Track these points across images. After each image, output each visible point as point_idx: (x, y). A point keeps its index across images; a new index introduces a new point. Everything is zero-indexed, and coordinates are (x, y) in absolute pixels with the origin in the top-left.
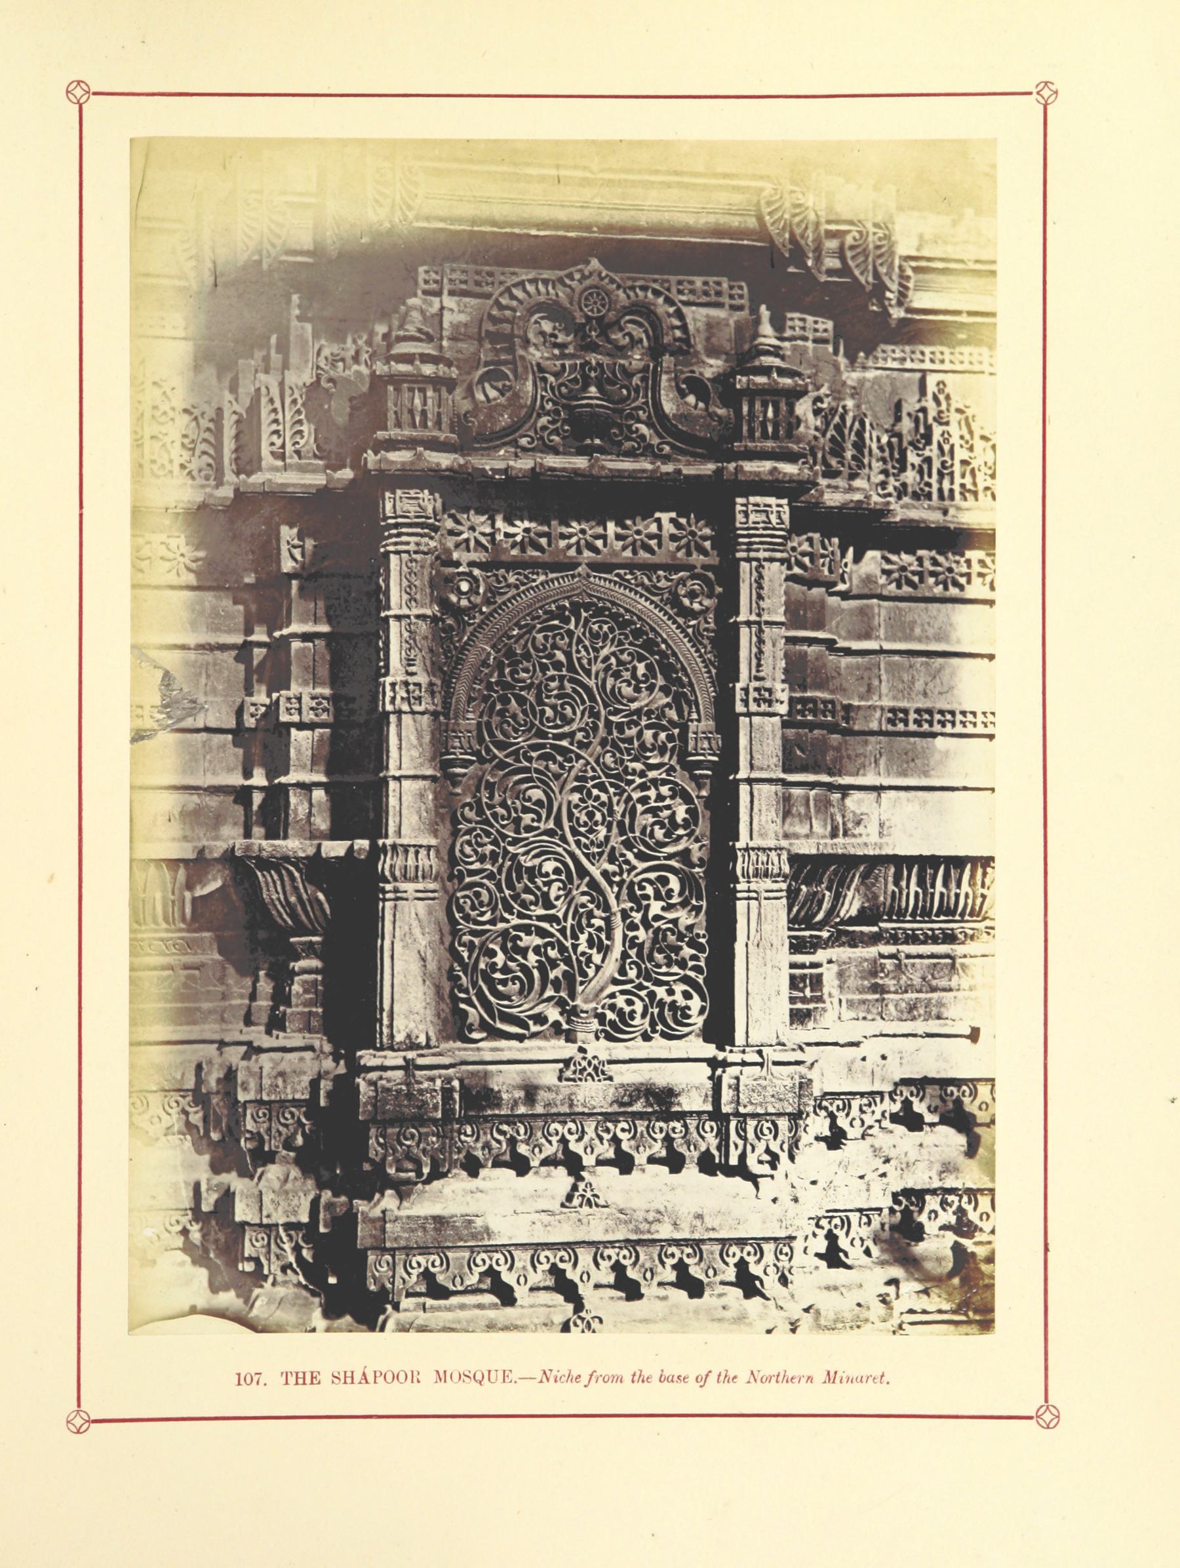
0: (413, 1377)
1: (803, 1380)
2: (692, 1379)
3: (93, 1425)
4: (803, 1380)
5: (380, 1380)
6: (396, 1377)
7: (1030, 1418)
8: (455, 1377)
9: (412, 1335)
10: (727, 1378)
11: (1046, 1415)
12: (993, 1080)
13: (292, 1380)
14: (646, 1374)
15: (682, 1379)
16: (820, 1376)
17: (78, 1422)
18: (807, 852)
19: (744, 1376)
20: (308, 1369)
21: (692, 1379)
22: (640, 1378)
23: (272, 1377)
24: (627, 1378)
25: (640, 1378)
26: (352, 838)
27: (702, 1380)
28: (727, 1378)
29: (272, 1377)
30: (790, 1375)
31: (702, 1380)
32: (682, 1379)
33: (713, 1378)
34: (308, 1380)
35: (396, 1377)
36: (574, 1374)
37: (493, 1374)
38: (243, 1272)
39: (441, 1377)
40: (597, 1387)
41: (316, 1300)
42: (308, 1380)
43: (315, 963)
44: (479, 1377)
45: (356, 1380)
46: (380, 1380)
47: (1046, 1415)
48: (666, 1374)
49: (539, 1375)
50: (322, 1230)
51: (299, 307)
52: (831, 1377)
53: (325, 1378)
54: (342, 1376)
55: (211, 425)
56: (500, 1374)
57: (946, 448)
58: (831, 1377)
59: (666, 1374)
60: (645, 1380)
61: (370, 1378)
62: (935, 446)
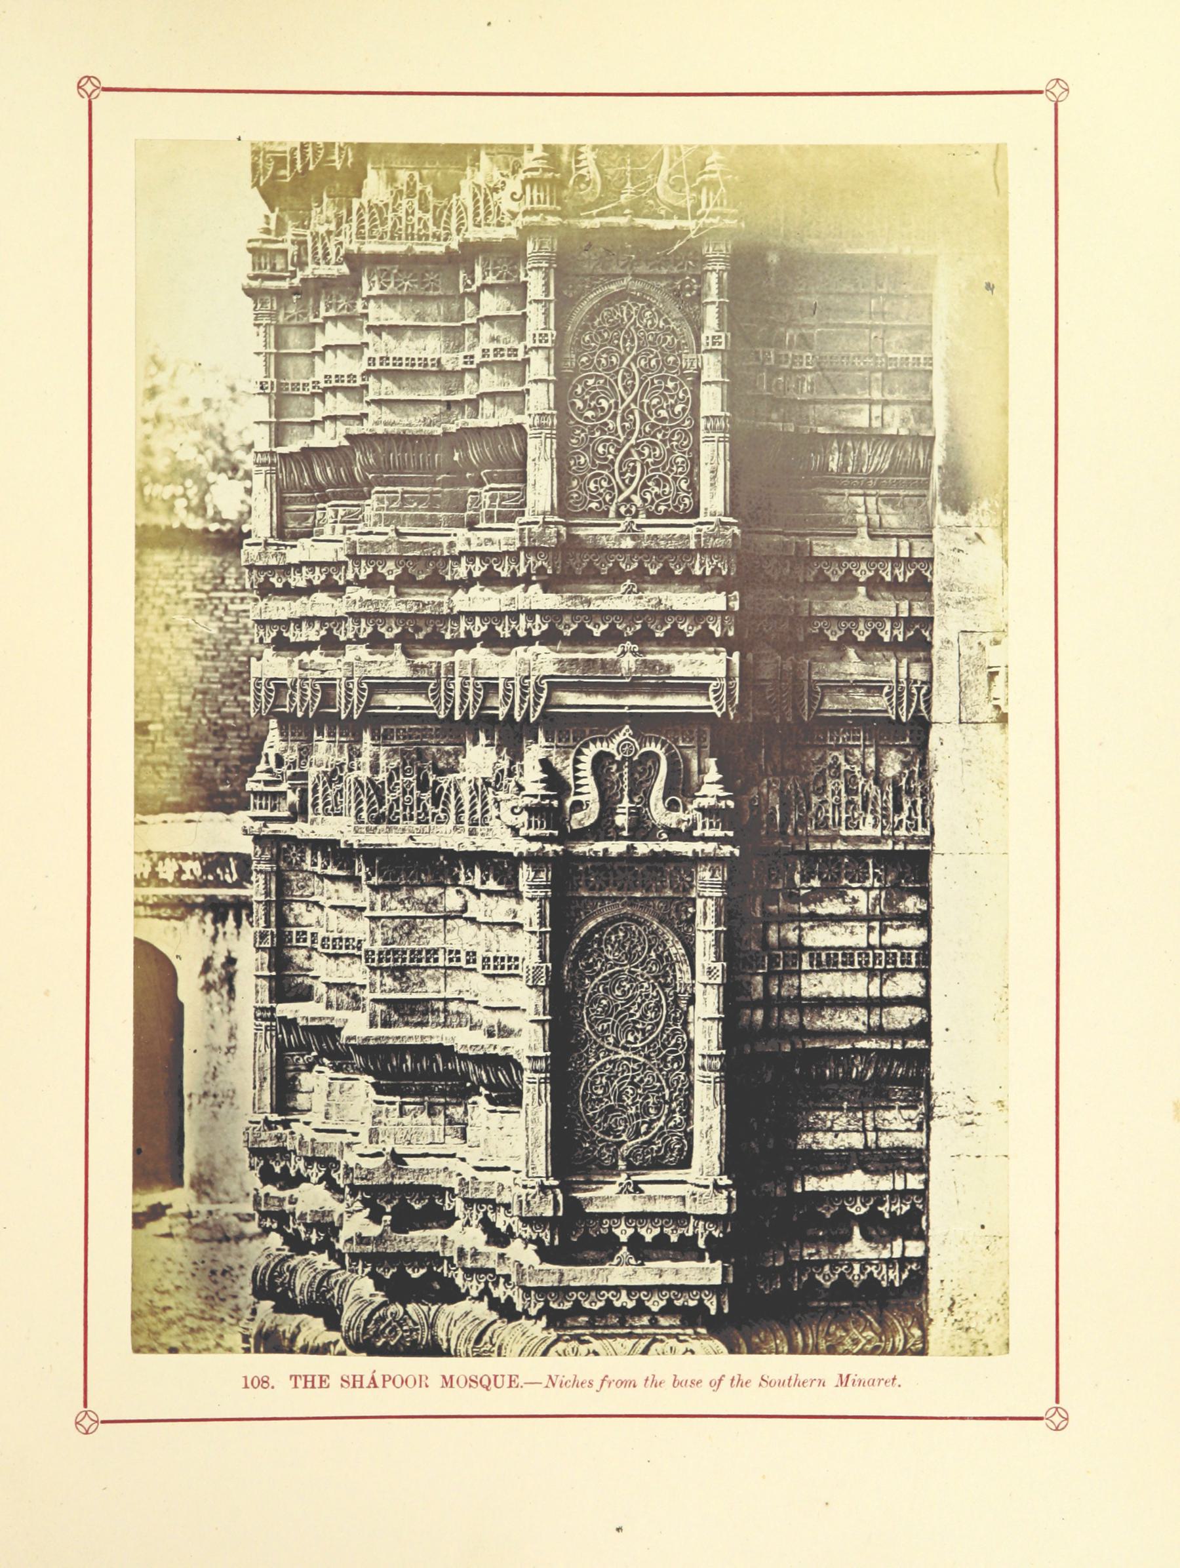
1: (815, 1383)
2: (706, 1383)
3: (86, 99)
4: (815, 1383)
5: (389, 1384)
6: (405, 1382)
7: (85, 1405)
8: (398, 1382)
11: (1056, 1417)
13: (301, 1383)
14: (744, 1379)
15: (696, 1383)
17: (1057, 1419)
20: (317, 1373)
21: (706, 1383)
24: (640, 1382)
26: (893, 850)
30: (801, 1378)
32: (696, 1383)
33: (726, 1383)
34: (317, 1383)
35: (405, 1382)
37: (499, 1379)
42: (317, 1383)
44: (485, 1382)
45: (366, 1384)
46: (389, 1384)
48: (679, 1378)
49: (545, 1380)
51: (445, 434)
56: (507, 1379)
59: (679, 1378)
60: (657, 1384)
61: (379, 1382)
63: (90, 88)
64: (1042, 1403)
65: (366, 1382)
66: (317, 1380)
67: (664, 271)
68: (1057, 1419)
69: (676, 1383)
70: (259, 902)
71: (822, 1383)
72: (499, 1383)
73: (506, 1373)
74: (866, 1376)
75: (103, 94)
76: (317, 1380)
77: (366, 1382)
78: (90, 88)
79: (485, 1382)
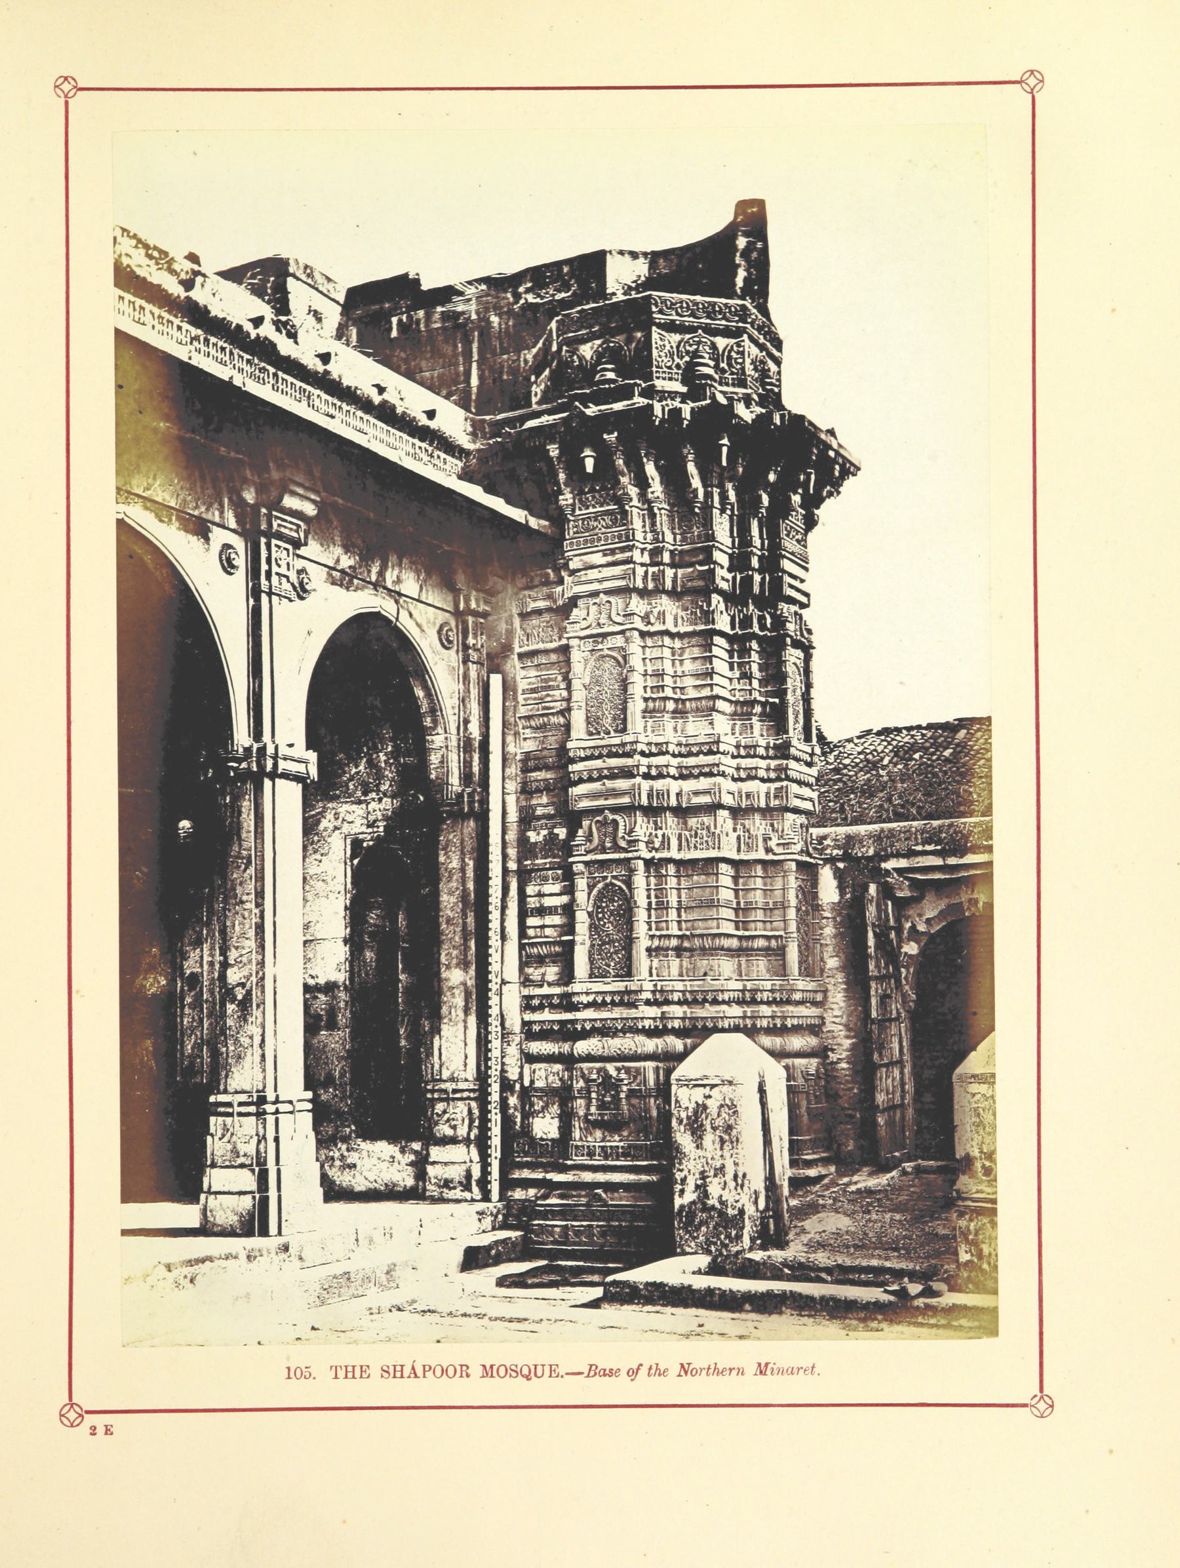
0: (464, 1370)
3: (63, 100)
4: (734, 1372)
8: (438, 1371)
9: (508, 1317)
10: (658, 1371)
12: (73, 1412)
13: (341, 1374)
17: (1042, 1406)
18: (608, 285)
20: (358, 1364)
27: (633, 1373)
28: (658, 1371)
31: (633, 1373)
32: (611, 1373)
33: (643, 1371)
34: (357, 1374)
35: (444, 1371)
41: (538, 1136)
42: (357, 1374)
44: (525, 1371)
45: (406, 1374)
46: (429, 1374)
47: (1030, 82)
50: (505, 377)
53: (375, 1371)
56: (547, 1369)
60: (662, 1373)
61: (420, 1372)
63: (69, 88)
64: (1026, 1390)
66: (358, 1370)
67: (762, 340)
68: (1042, 1406)
69: (685, 1369)
70: (543, 975)
71: (741, 1372)
72: (539, 1373)
73: (547, 1362)
74: (784, 1363)
76: (358, 1370)
78: (69, 88)
79: (525, 1371)
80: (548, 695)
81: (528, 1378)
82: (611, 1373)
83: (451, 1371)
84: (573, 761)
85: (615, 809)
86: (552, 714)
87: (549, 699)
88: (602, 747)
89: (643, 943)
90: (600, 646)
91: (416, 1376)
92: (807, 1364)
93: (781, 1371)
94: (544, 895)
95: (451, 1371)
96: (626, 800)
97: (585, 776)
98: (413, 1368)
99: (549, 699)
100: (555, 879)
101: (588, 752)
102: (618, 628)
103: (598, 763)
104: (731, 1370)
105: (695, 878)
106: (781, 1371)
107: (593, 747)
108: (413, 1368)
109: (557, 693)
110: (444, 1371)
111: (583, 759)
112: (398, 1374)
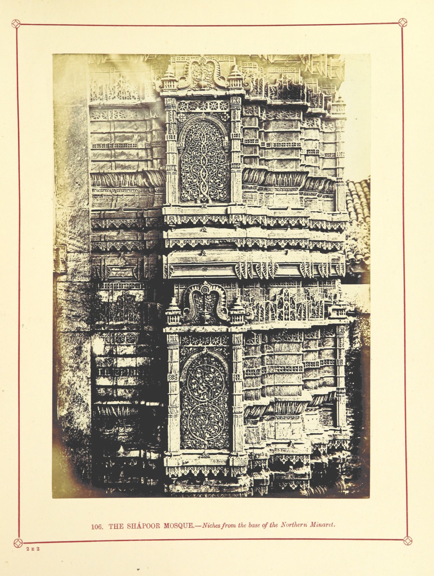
0: (157, 526)
4: (303, 526)
5: (145, 527)
10: (273, 525)
13: (113, 527)
15: (257, 526)
16: (309, 524)
19: (280, 524)
20: (119, 523)
22: (241, 525)
23: (106, 526)
24: (237, 526)
25: (241, 525)
27: (265, 526)
28: (273, 525)
29: (106, 526)
31: (265, 526)
32: (257, 526)
33: (268, 525)
34: (119, 527)
35: (151, 526)
36: (275, 523)
37: (185, 525)
38: (150, 459)
39: (167, 526)
40: (226, 529)
42: (119, 527)
43: (131, 381)
44: (180, 525)
45: (136, 527)
46: (145, 527)
49: (202, 525)
52: (313, 525)
53: (125, 526)
54: (131, 526)
55: (133, 177)
56: (188, 525)
57: (287, 294)
58: (313, 525)
59: (251, 524)
60: (276, 526)
61: (142, 526)
62: (283, 294)
65: (137, 526)
71: (305, 525)
72: (185, 526)
75: (21, 538)
77: (137, 526)
79: (180, 525)
80: (123, 154)
81: (181, 528)
82: (233, 526)
83: (148, 526)
84: (167, 228)
85: (214, 280)
86: (131, 174)
87: (123, 158)
88: (202, 215)
89: (240, 369)
90: (198, 110)
91: (140, 528)
92: (330, 523)
93: (320, 525)
94: (117, 356)
95: (153, 526)
96: (228, 272)
97: (182, 244)
98: (139, 525)
99: (123, 158)
100: (131, 340)
101: (186, 220)
102: (222, 93)
103: (196, 232)
104: (301, 524)
105: (277, 346)
106: (320, 525)
107: (193, 215)
108: (139, 525)
109: (134, 152)
110: (151, 526)
111: (178, 226)
112: (134, 527)
